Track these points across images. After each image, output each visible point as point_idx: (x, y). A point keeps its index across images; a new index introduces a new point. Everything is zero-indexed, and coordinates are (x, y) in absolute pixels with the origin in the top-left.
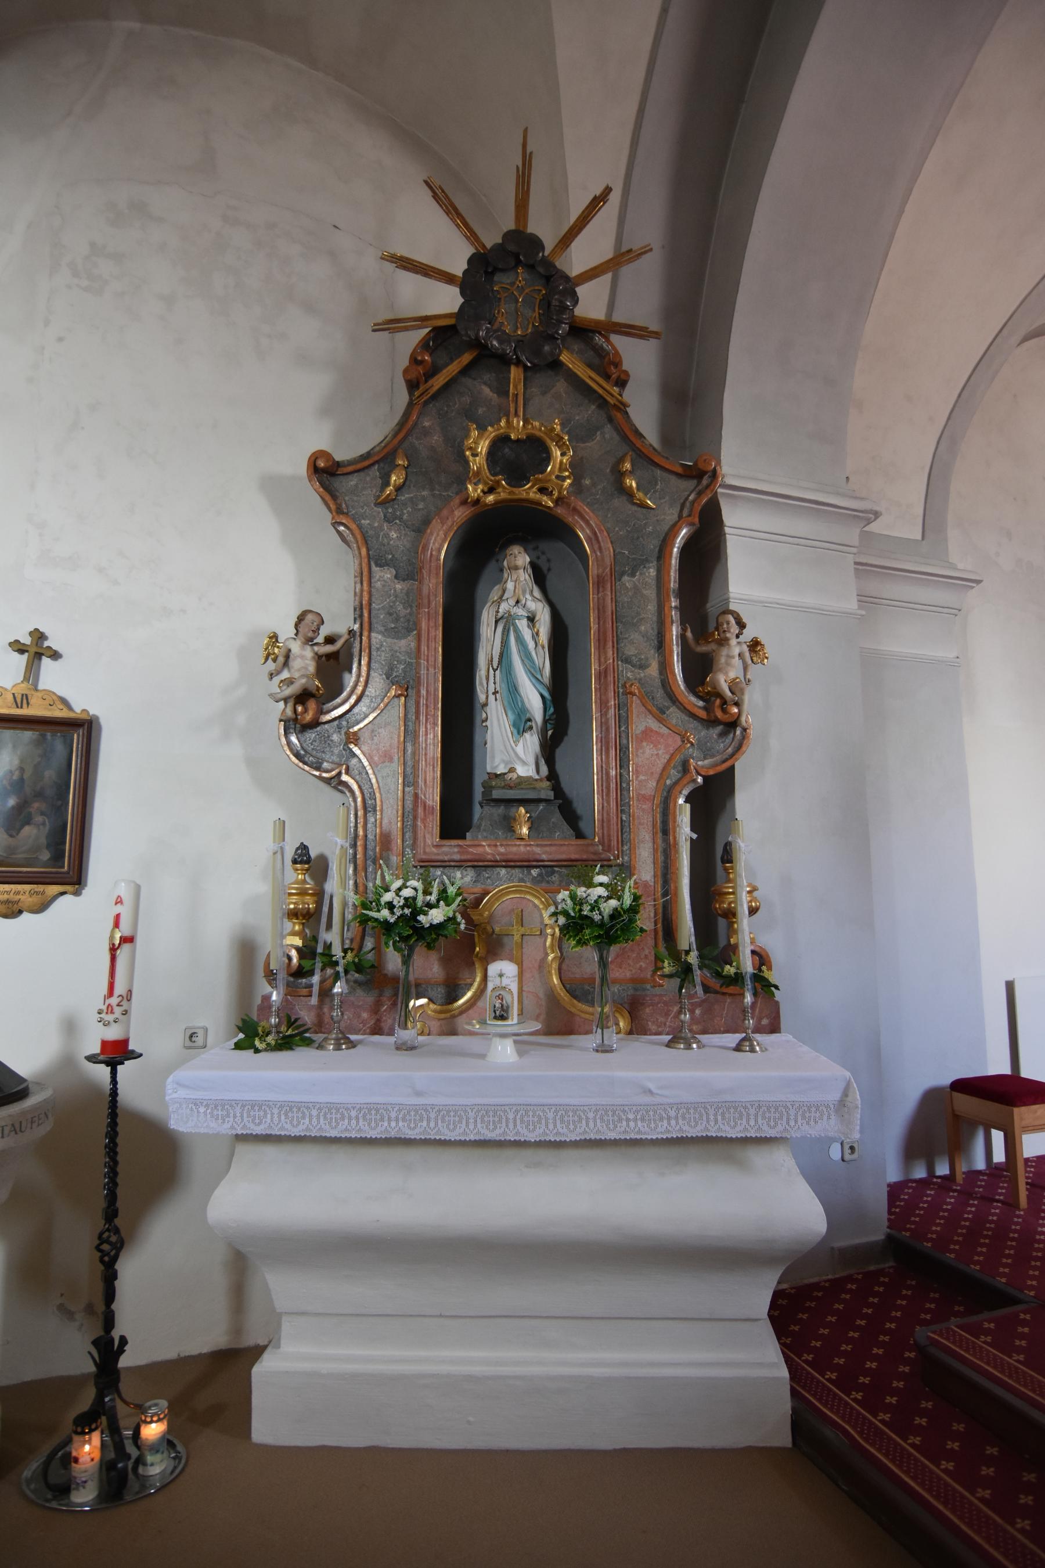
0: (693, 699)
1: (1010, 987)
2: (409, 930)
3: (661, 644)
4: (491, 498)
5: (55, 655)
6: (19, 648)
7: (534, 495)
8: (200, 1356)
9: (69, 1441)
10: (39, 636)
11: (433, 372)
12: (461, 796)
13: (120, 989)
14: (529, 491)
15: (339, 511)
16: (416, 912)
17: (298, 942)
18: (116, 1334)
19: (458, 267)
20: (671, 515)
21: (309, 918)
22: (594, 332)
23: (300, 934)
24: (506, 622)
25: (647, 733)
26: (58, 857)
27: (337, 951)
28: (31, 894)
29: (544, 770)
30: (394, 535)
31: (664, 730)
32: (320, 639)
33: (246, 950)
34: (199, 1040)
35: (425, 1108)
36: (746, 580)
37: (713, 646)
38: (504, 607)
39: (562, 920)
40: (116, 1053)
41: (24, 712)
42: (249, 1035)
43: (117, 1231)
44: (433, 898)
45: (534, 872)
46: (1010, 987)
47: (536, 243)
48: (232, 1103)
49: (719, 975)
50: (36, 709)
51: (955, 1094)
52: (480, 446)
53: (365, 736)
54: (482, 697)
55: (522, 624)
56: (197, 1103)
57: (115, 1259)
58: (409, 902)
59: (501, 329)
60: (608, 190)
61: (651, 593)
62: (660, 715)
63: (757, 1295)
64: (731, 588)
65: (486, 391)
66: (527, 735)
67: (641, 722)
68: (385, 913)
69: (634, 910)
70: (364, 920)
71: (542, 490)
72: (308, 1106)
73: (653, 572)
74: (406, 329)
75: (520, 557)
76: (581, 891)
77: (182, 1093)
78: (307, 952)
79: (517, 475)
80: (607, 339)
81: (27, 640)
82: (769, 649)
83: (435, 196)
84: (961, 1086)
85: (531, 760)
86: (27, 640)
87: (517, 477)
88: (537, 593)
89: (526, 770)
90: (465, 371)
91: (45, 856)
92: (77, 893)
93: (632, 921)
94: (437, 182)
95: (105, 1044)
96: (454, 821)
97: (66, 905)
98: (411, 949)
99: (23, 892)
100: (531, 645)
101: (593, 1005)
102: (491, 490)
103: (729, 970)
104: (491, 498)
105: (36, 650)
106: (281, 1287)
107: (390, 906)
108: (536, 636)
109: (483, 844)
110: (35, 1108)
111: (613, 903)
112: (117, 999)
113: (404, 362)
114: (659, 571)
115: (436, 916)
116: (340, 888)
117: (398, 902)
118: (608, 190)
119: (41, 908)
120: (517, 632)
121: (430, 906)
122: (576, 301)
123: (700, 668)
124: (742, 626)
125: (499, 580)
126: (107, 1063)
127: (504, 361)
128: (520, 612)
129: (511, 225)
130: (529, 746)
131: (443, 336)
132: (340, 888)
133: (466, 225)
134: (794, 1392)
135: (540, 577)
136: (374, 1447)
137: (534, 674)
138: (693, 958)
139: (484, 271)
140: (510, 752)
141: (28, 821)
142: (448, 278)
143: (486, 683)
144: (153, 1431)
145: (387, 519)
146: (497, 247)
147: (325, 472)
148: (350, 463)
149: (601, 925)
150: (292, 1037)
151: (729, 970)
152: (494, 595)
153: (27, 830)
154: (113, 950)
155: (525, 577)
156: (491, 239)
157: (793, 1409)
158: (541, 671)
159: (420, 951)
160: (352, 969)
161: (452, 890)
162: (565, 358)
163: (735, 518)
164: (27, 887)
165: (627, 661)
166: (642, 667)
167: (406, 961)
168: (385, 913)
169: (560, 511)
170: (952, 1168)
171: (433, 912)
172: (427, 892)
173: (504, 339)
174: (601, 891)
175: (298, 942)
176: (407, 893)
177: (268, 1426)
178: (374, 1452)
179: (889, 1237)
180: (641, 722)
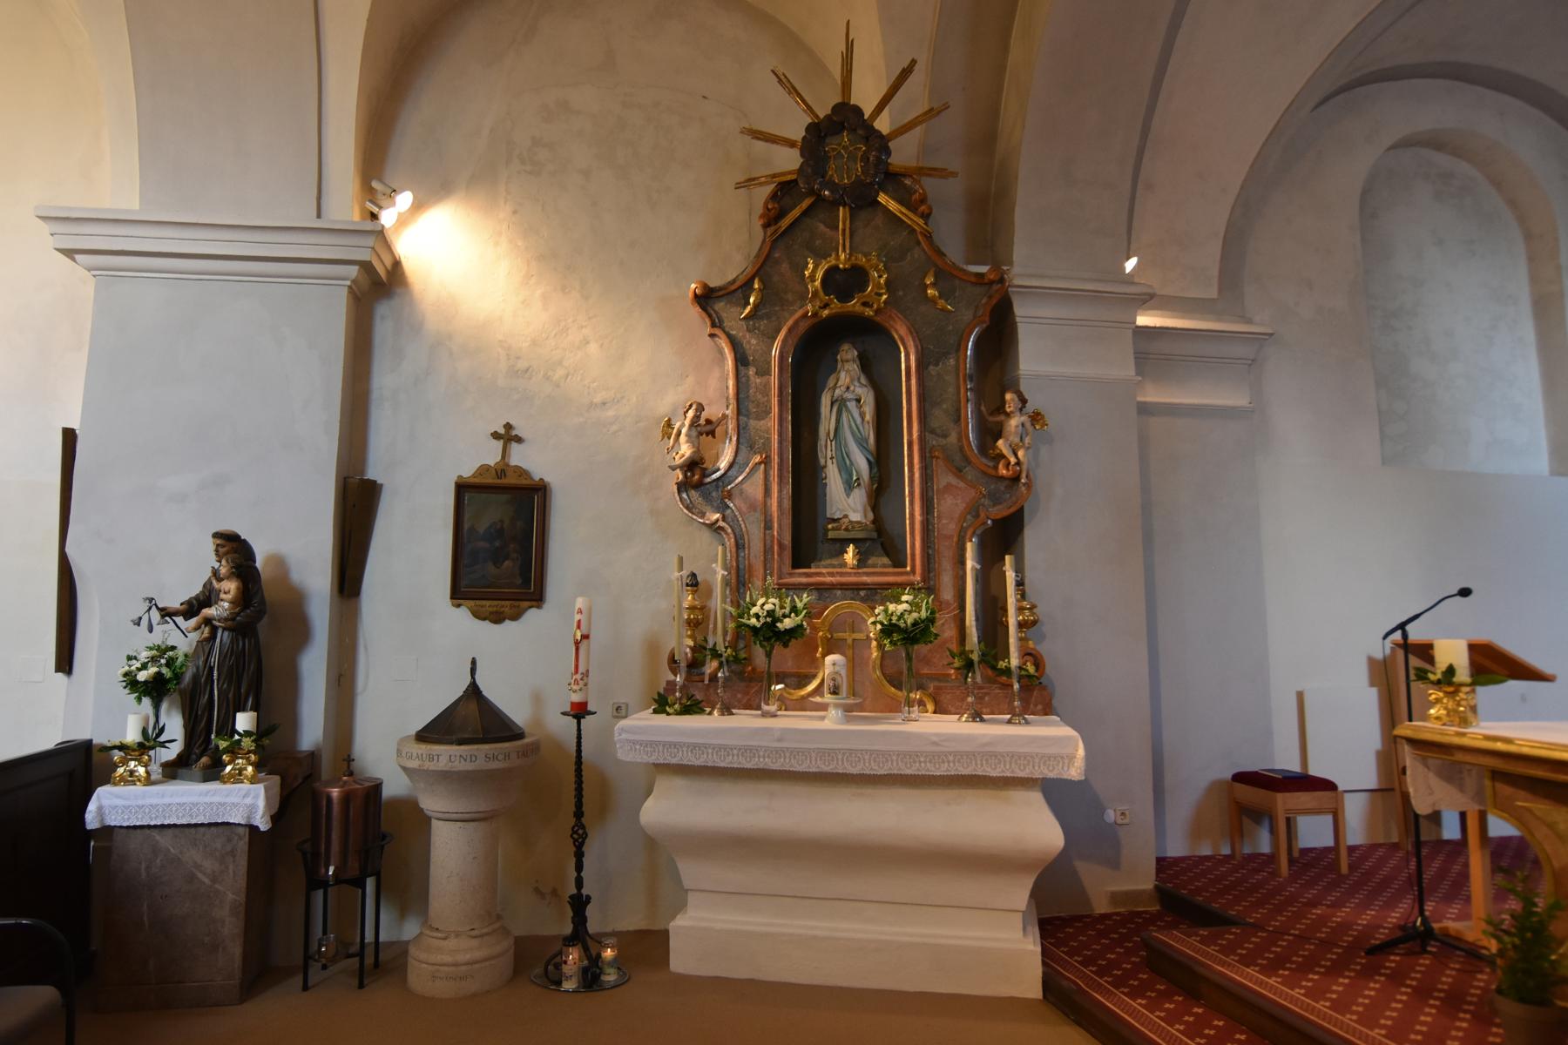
0: (984, 460)
1: (1300, 696)
2: (770, 633)
3: (958, 418)
4: (826, 312)
5: (519, 440)
6: (496, 436)
7: (859, 309)
8: (628, 932)
9: (560, 953)
10: (508, 427)
11: (781, 215)
12: (808, 536)
13: (582, 669)
14: (854, 305)
15: (713, 325)
16: (776, 620)
17: (691, 643)
18: (584, 892)
19: (798, 134)
20: (967, 315)
21: (697, 622)
22: (904, 176)
23: (692, 637)
24: (840, 404)
25: (948, 487)
26: (527, 582)
27: (721, 648)
28: (512, 607)
29: (871, 516)
30: (754, 341)
31: (962, 485)
32: (702, 421)
33: (652, 647)
34: (623, 712)
35: (782, 749)
36: (1034, 357)
37: (1002, 417)
38: (838, 392)
39: (879, 627)
40: (580, 712)
41: (504, 481)
42: (661, 704)
43: (583, 827)
44: (787, 611)
45: (862, 593)
46: (1300, 696)
47: (858, 111)
48: (657, 743)
49: (994, 668)
50: (511, 480)
51: (1237, 785)
52: (815, 271)
53: (736, 493)
54: (822, 462)
55: (852, 405)
56: (634, 742)
57: (582, 844)
58: (770, 613)
59: (836, 173)
60: (914, 62)
61: (950, 378)
62: (958, 472)
63: (1018, 894)
64: (1022, 366)
65: (822, 227)
66: (856, 491)
67: (944, 478)
68: (753, 621)
69: (931, 620)
70: (740, 626)
71: (865, 304)
72: (706, 746)
73: (952, 362)
74: (761, 184)
75: (848, 353)
76: (892, 607)
77: (624, 736)
78: (698, 649)
79: (845, 297)
80: (918, 182)
81: (502, 431)
82: (1052, 418)
83: (780, 81)
84: (1240, 777)
85: (860, 508)
86: (502, 431)
87: (845, 297)
88: (863, 380)
89: (855, 517)
90: (805, 213)
91: (519, 581)
92: (539, 607)
93: (927, 628)
94: (780, 70)
95: (573, 704)
96: (802, 555)
97: (532, 615)
98: (772, 648)
99: (506, 605)
100: (859, 421)
101: (900, 689)
102: (825, 306)
103: (1002, 664)
104: (826, 312)
105: (508, 436)
106: (691, 872)
107: (757, 616)
108: (862, 415)
109: (823, 572)
110: (527, 745)
111: (915, 615)
112: (582, 676)
113: (759, 209)
114: (957, 361)
115: (787, 623)
116: (719, 603)
117: (762, 614)
118: (914, 62)
119: (515, 617)
120: (848, 411)
121: (785, 616)
122: (889, 153)
123: (990, 432)
124: (1024, 401)
125: (833, 369)
126: (574, 717)
127: (835, 204)
128: (849, 395)
129: (838, 99)
130: (859, 498)
131: (785, 190)
132: (719, 603)
133: (804, 101)
134: (1044, 963)
135: (866, 365)
136: (752, 980)
137: (862, 443)
138: (975, 657)
139: (818, 135)
140: (846, 504)
141: (507, 558)
142: (791, 144)
143: (827, 453)
144: (609, 953)
145: (748, 330)
146: (828, 117)
147: (706, 298)
148: (721, 289)
149: (905, 631)
150: (691, 708)
151: (1002, 664)
152: (831, 382)
153: (507, 563)
154: (577, 643)
155: (854, 367)
156: (823, 111)
157: (1044, 973)
158: (867, 441)
159: (778, 649)
160: (728, 664)
161: (800, 605)
162: (882, 198)
163: (1020, 310)
164: (508, 603)
165: (933, 432)
166: (945, 436)
167: (768, 655)
168: (753, 621)
169: (878, 319)
170: (1233, 849)
171: (787, 621)
172: (782, 607)
173: (833, 186)
174: (905, 606)
175: (691, 643)
176: (768, 607)
177: (681, 961)
178: (751, 981)
179: (1156, 887)
180: (944, 478)
